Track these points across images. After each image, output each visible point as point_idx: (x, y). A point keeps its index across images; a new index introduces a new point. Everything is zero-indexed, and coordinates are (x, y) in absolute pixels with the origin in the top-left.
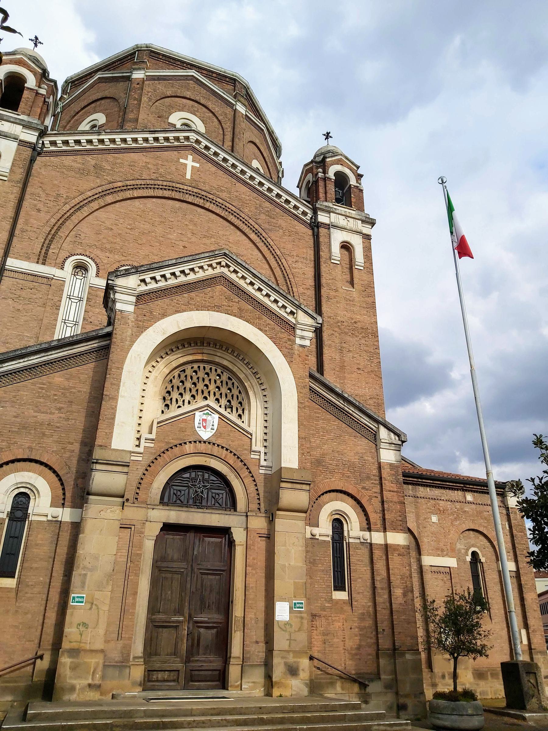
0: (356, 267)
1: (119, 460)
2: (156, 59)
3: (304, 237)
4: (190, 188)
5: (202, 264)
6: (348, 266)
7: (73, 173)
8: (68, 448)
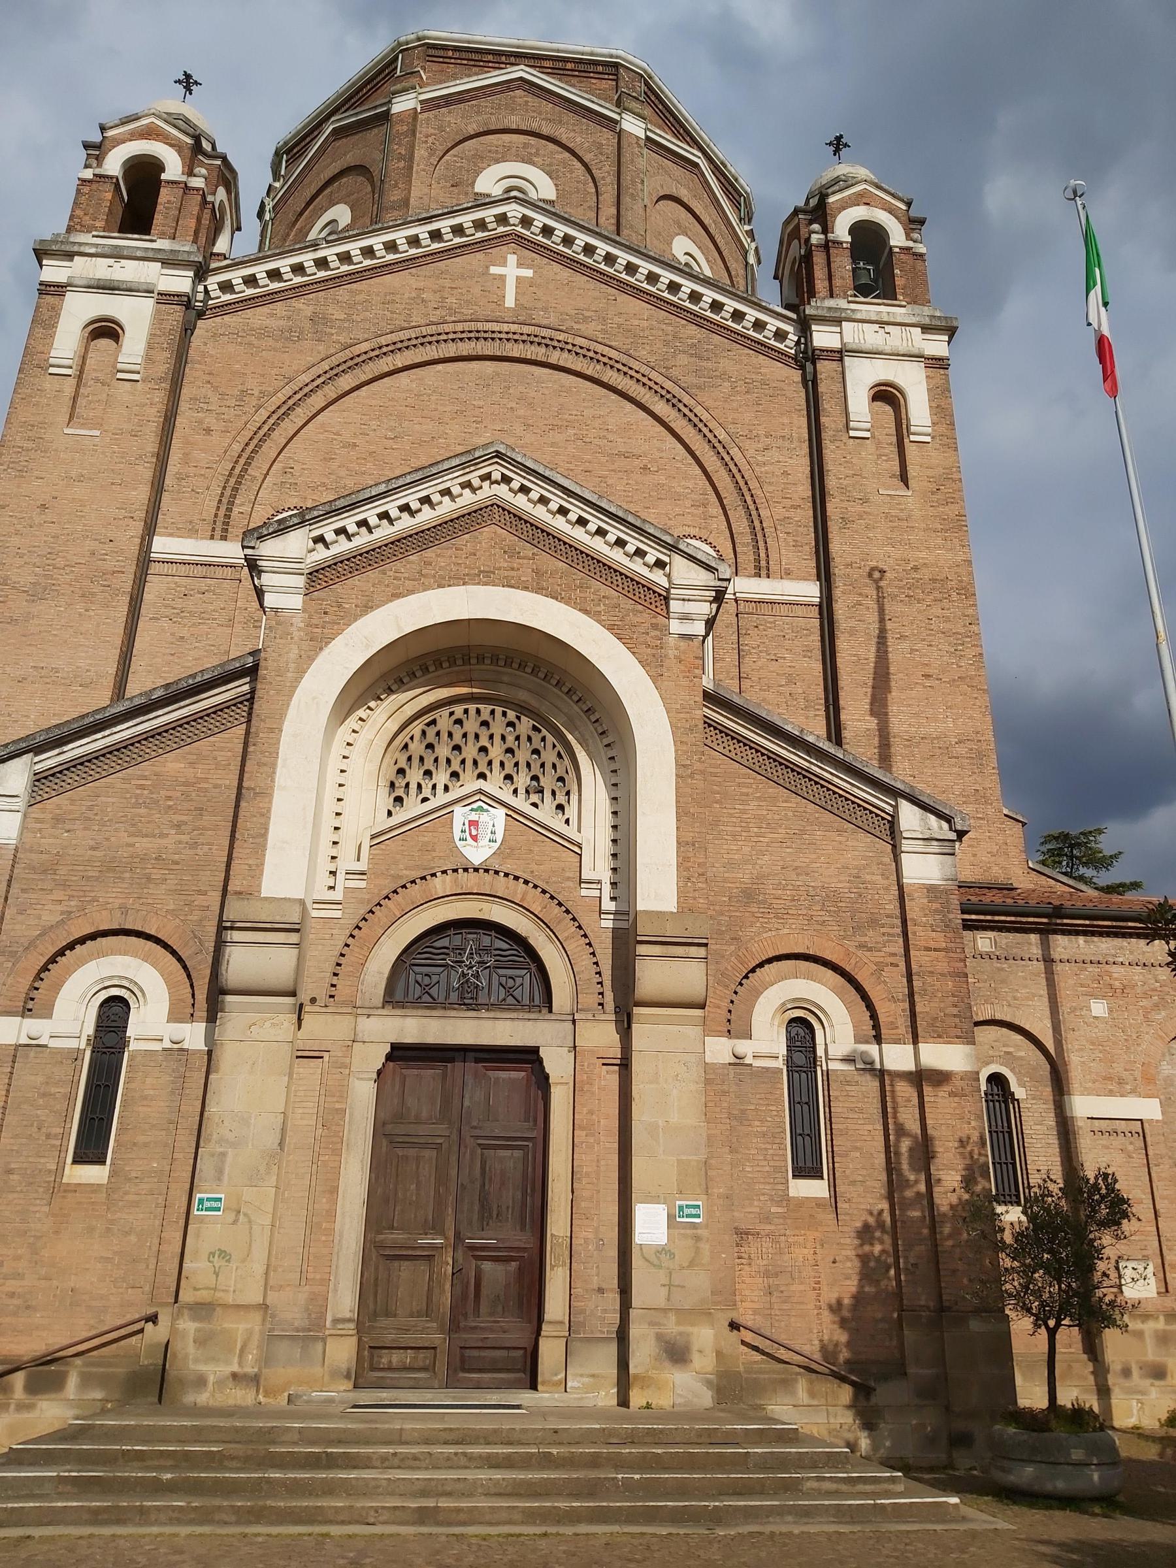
0: (913, 438)
2: (441, 60)
4: (514, 328)
5: (448, 484)
6: (894, 439)
7: (270, 342)
8: (196, 903)
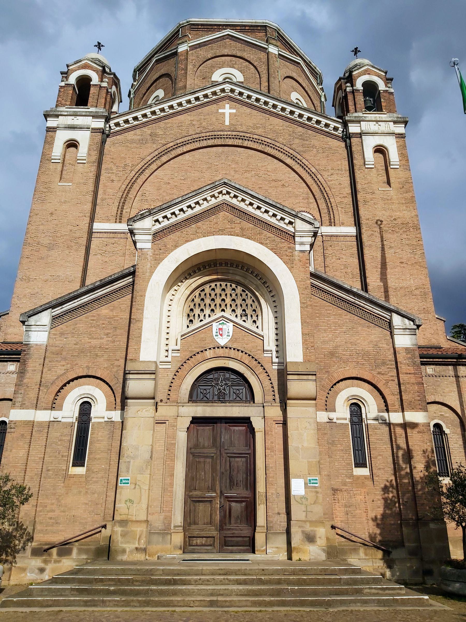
0: (392, 167)
1: (147, 369)
3: (337, 150)
5: (206, 196)
6: (384, 168)
7: (135, 145)
